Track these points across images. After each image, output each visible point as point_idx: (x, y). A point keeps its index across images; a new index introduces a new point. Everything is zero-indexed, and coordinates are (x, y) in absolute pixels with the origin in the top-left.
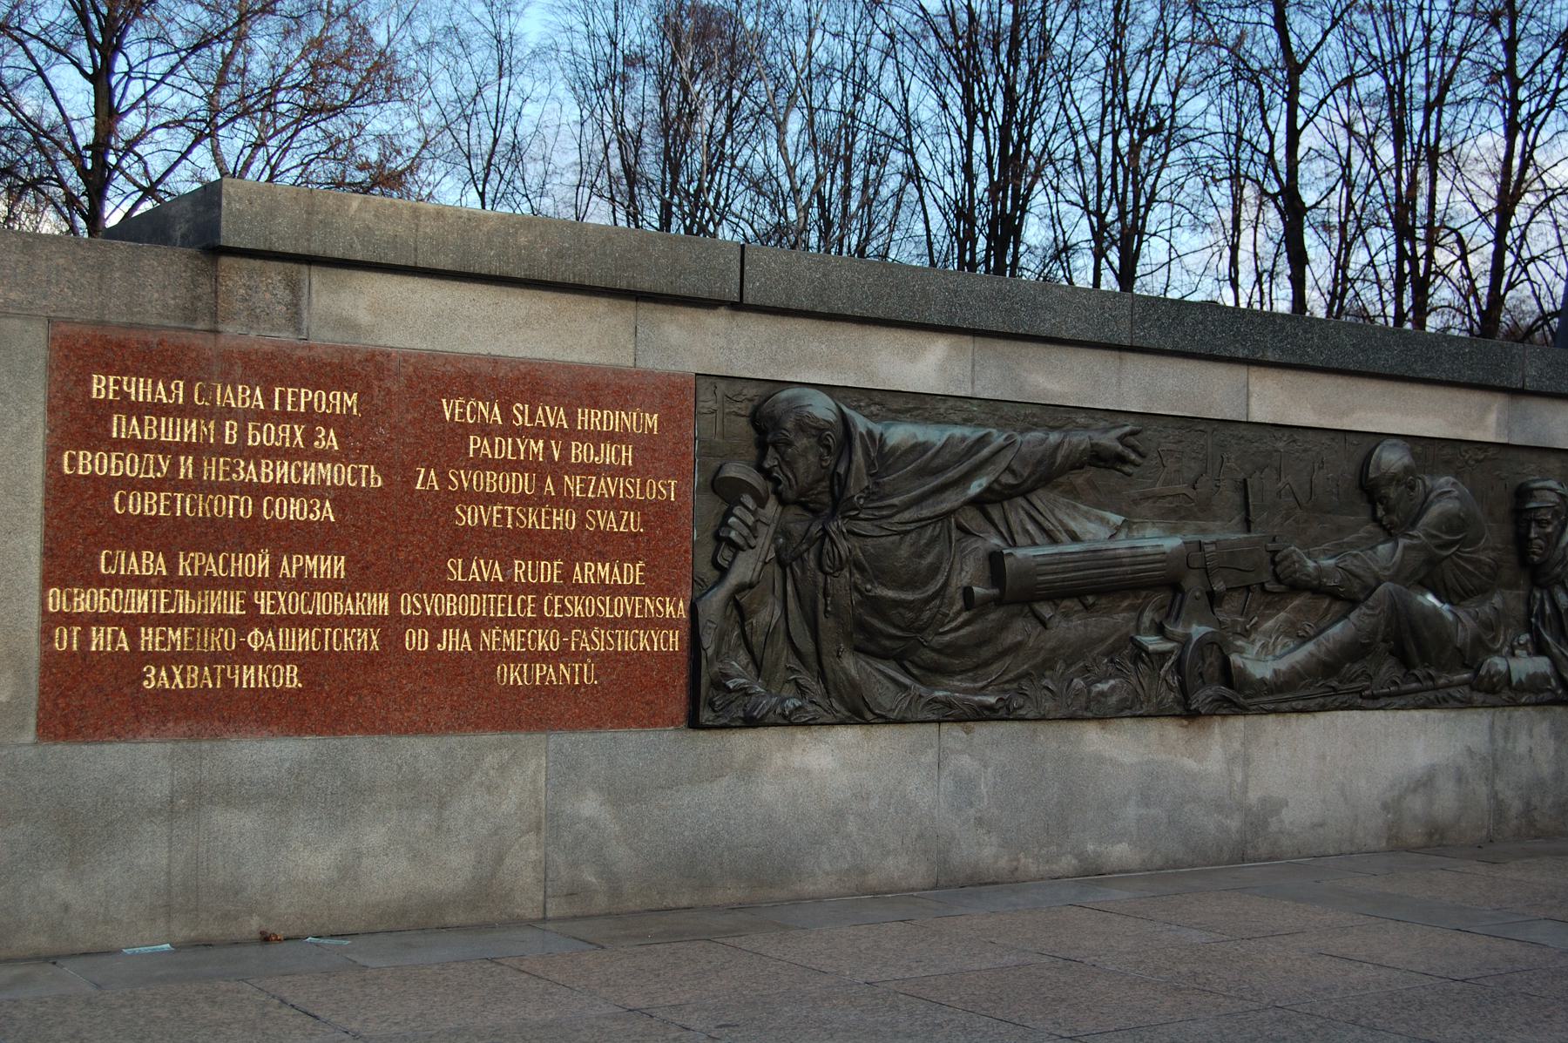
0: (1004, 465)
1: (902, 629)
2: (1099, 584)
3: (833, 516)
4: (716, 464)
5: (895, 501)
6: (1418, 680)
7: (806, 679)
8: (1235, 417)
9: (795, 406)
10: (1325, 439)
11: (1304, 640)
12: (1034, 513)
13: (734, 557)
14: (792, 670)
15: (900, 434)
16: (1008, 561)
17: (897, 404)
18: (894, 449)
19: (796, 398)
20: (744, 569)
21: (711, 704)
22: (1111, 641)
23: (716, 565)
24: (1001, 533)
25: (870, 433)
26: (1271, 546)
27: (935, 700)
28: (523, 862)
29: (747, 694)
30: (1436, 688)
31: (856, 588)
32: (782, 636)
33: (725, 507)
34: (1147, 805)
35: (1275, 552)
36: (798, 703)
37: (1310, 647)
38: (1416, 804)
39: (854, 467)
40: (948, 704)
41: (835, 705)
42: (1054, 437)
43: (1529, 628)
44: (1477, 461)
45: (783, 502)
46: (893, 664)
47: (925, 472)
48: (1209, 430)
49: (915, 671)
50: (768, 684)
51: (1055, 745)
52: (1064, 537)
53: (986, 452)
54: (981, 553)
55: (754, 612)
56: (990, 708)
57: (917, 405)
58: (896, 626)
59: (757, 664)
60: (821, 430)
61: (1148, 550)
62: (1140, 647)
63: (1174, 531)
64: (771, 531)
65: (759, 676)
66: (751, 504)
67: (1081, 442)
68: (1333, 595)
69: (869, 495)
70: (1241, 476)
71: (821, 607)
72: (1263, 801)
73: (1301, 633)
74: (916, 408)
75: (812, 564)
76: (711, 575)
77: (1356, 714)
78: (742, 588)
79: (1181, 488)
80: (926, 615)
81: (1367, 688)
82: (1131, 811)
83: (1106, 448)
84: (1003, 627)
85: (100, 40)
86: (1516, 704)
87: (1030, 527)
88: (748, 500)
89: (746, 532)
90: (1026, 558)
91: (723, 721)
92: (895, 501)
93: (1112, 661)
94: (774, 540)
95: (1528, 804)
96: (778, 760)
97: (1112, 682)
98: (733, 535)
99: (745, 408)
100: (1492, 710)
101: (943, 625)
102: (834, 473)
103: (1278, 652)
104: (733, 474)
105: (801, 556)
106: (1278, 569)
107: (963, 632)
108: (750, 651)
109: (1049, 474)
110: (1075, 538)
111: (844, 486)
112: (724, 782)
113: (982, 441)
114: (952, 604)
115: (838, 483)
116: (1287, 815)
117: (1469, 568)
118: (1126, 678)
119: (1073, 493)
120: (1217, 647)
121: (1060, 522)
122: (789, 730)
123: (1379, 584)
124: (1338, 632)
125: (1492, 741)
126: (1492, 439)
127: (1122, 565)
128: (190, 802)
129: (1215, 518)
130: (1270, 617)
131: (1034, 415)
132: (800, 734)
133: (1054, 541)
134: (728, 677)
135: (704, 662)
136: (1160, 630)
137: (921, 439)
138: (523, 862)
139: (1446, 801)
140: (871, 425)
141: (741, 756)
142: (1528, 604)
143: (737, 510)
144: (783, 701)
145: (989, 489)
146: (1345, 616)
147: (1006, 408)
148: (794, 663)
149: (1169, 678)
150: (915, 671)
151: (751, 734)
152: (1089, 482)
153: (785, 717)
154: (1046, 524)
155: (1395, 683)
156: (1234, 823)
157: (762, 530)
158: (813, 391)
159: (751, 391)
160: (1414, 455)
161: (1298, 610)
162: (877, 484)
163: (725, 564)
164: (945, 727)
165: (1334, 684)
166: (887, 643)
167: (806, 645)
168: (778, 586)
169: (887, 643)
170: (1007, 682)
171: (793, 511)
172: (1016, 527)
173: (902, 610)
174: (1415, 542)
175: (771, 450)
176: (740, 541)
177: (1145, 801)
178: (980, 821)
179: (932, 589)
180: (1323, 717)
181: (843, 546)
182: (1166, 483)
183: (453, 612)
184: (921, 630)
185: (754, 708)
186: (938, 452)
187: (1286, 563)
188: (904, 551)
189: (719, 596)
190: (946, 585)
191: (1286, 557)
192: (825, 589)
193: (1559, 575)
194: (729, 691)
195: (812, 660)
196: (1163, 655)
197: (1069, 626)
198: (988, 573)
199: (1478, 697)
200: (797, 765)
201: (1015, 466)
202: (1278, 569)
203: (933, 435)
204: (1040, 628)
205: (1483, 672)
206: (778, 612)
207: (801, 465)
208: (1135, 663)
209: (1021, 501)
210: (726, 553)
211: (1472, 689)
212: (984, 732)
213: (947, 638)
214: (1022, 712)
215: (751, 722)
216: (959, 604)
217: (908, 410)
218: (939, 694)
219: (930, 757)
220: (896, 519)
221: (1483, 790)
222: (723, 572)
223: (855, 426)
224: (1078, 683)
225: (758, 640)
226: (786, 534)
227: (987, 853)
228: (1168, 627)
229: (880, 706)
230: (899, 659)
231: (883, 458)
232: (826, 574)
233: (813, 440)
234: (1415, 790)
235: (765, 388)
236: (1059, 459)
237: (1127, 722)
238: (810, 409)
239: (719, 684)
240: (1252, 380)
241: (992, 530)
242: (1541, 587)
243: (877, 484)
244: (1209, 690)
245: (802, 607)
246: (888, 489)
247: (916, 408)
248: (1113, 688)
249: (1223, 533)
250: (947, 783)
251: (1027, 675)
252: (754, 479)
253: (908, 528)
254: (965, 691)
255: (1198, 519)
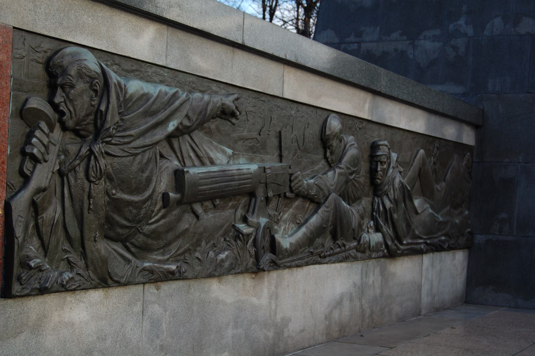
0: (185, 113)
1: (129, 221)
3: (95, 139)
4: (24, 97)
5: (132, 132)
6: (340, 247)
7: (74, 257)
8: (278, 95)
9: (77, 60)
10: (309, 110)
11: (300, 226)
12: (194, 145)
13: (34, 167)
14: (65, 251)
15: (135, 86)
16: (186, 176)
17: (237, 45)
18: (132, 96)
19: (77, 54)
20: (41, 176)
21: (19, 279)
22: (225, 227)
23: (22, 173)
24: (178, 157)
25: (119, 84)
26: (290, 171)
27: (144, 269)
29: (41, 271)
30: (345, 251)
31: (107, 193)
32: (60, 227)
33: (28, 130)
34: (237, 328)
35: (291, 175)
36: (71, 276)
37: (304, 229)
38: (336, 315)
39: (111, 107)
40: (151, 271)
41: (92, 275)
42: (206, 97)
43: (373, 218)
44: (360, 129)
45: (64, 128)
46: (120, 244)
47: (149, 113)
48: (266, 101)
49: (133, 249)
50: (51, 263)
51: (198, 294)
52: (208, 162)
53: (177, 103)
54: (171, 170)
55: (45, 209)
56: (172, 273)
58: (126, 219)
59: (45, 247)
60: (92, 78)
61: (245, 171)
62: (238, 231)
63: (251, 160)
64: (57, 150)
65: (45, 256)
66: (46, 129)
67: (218, 101)
68: (312, 200)
69: (118, 126)
70: (278, 129)
71: (86, 205)
72: (282, 319)
73: (298, 222)
74: (137, 70)
75: (81, 175)
76: (17, 181)
77: (317, 266)
78: (40, 190)
79: (255, 134)
80: (143, 211)
81: (322, 252)
82: (230, 332)
83: (228, 107)
84: (179, 219)
86: (370, 258)
87: (192, 154)
88: (43, 125)
89: (43, 149)
90: (194, 174)
91: (26, 292)
92: (132, 132)
93: (225, 240)
94: (59, 156)
95: (372, 310)
96: (55, 317)
97: (226, 253)
98: (35, 151)
99: (41, 57)
100: (362, 262)
101: (151, 219)
102: (98, 110)
103: (289, 233)
104: (35, 106)
105: (74, 169)
106: (292, 184)
107: (161, 222)
108: (40, 238)
110: (212, 163)
111: (104, 121)
112: (23, 337)
113: (175, 96)
114: (156, 204)
115: (99, 117)
116: (294, 327)
117: (357, 185)
118: (232, 250)
119: (209, 133)
120: (269, 230)
121: (205, 151)
122: (63, 295)
123: (330, 194)
124: (314, 220)
125: (362, 278)
126: (366, 116)
127: (235, 181)
129: (267, 153)
130: (286, 211)
131: (193, 83)
132: (69, 297)
133: (203, 164)
134: (30, 258)
135: (16, 247)
136: (245, 220)
137: (146, 91)
140: (119, 79)
141: (33, 317)
142: (372, 205)
143: (38, 133)
144: (61, 274)
145: (177, 129)
146: (316, 212)
147: (181, 75)
148: (67, 246)
149: (251, 249)
150: (133, 249)
151: (40, 299)
152: (217, 128)
153: (63, 286)
154: (199, 153)
155: (332, 249)
156: (271, 334)
157: (52, 148)
158: (85, 50)
159: (46, 45)
160: (342, 123)
161: (297, 208)
162: (122, 120)
163: (28, 173)
164: (147, 286)
165: (312, 250)
166: (120, 231)
167: (74, 231)
168: (58, 190)
169: (120, 231)
170: (179, 255)
171: (69, 135)
172: (185, 155)
173: (131, 208)
174: (342, 171)
175: (59, 91)
176: (39, 156)
177: (236, 327)
178: (162, 348)
179: (147, 194)
180: (306, 269)
181: (102, 162)
182: (249, 131)
184: (139, 222)
185: (46, 281)
186: (154, 101)
187: (296, 181)
188: (135, 168)
189: (25, 196)
190: (154, 191)
191: (296, 178)
192: (89, 192)
193: (386, 191)
194: (30, 268)
195: (77, 244)
196: (249, 235)
197: (210, 218)
198: (174, 184)
199: (359, 255)
200: (66, 320)
201: (190, 115)
202: (292, 184)
203: (153, 90)
204: (195, 220)
205: (362, 242)
206: (59, 210)
207: (78, 103)
208: (235, 241)
209: (187, 137)
210: (28, 165)
211: (357, 251)
212: (169, 288)
213: (153, 226)
214: (186, 274)
215: (43, 291)
216: (160, 204)
217: (133, 71)
218: (147, 264)
219: (138, 308)
220: (132, 145)
221: (358, 304)
222: (26, 179)
223: (111, 78)
224: (212, 254)
225: (45, 230)
226: (65, 152)
228: (250, 219)
229: (117, 275)
230: (123, 241)
231: (127, 103)
232: (90, 182)
233: (88, 85)
234: (336, 308)
235: (54, 45)
236: (208, 112)
237: (230, 277)
238: (86, 63)
239: (25, 265)
240: (285, 73)
241: (174, 155)
242: (378, 196)
243: (122, 120)
244: (265, 257)
245: (73, 205)
246: (128, 124)
247: (137, 70)
248: (227, 257)
249: (271, 163)
250: (146, 324)
251: (188, 250)
252: (48, 110)
253: (138, 151)
254: (159, 262)
255: (261, 153)
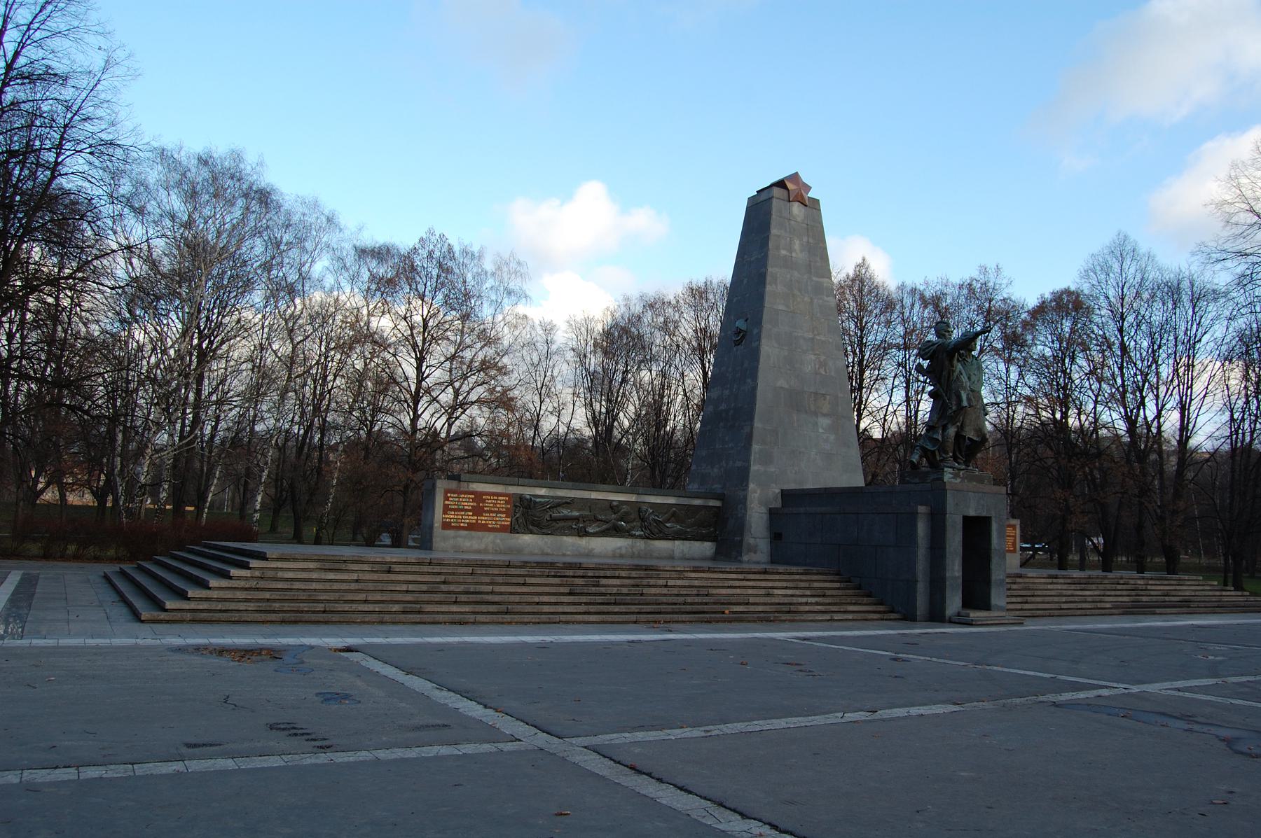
2: (566, 519)
28: (491, 546)
57: (542, 497)
85: (110, 498)
109: (559, 505)
128: (455, 537)
138: (491, 546)
139: (624, 551)
183: (483, 519)
197: (561, 524)
227: (549, 551)
244: (583, 533)
249: (587, 513)
